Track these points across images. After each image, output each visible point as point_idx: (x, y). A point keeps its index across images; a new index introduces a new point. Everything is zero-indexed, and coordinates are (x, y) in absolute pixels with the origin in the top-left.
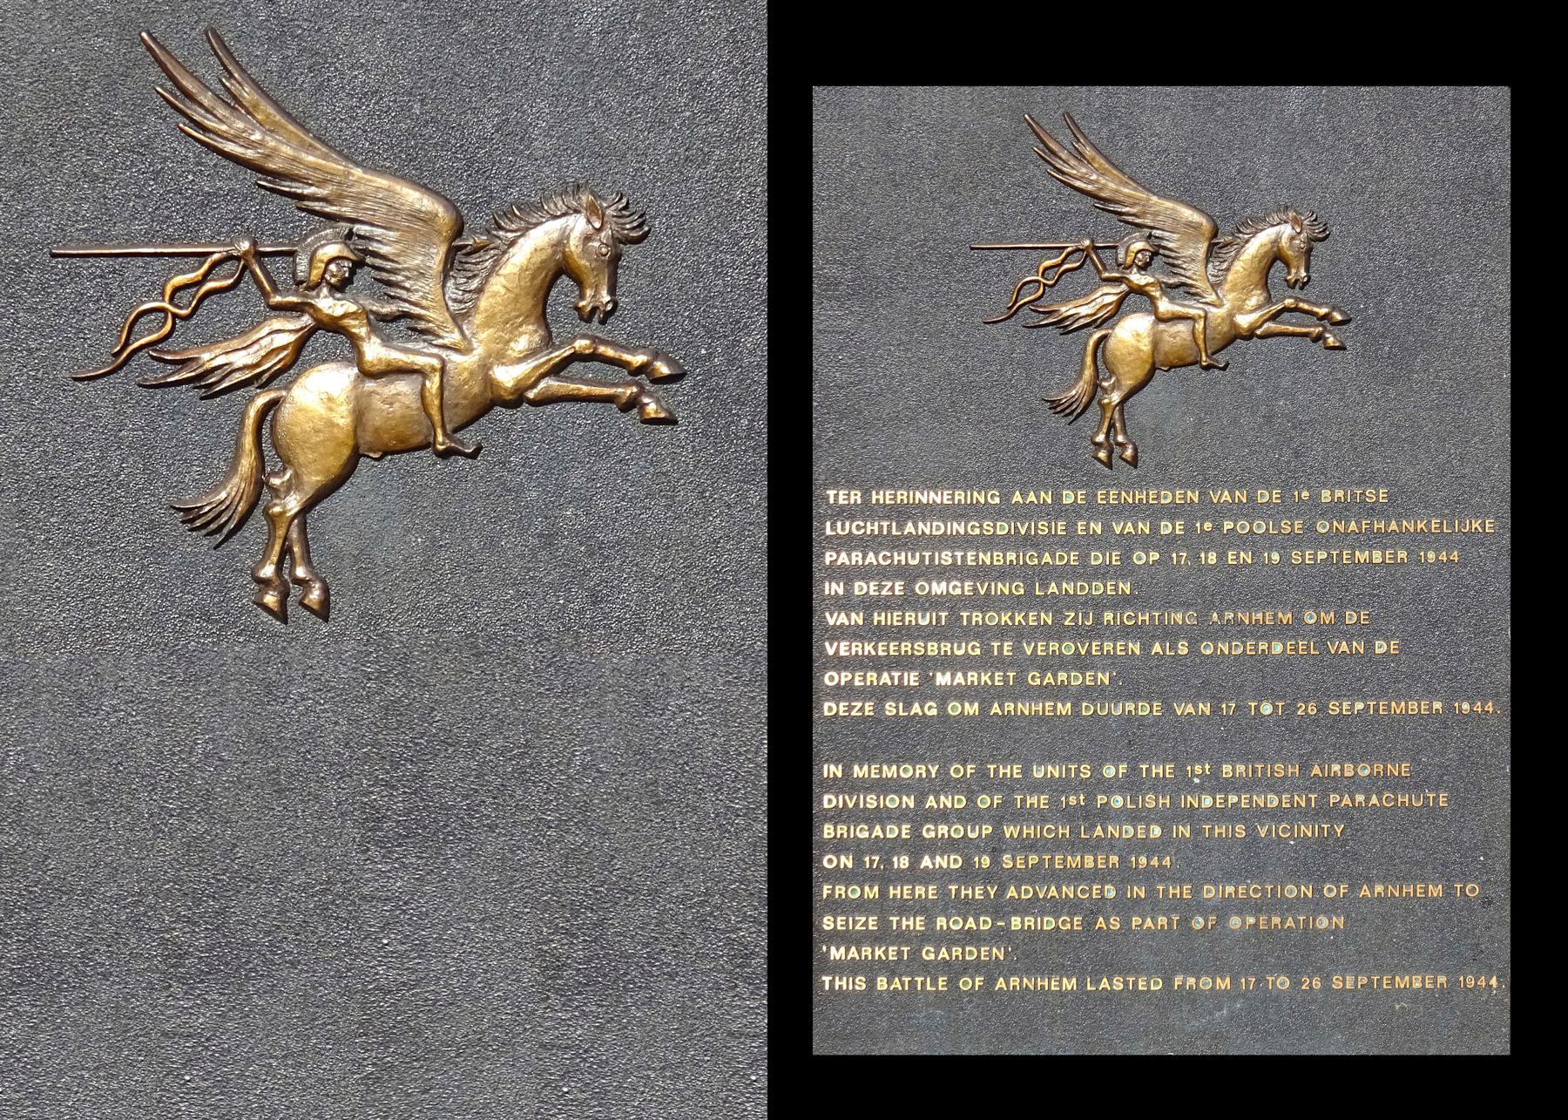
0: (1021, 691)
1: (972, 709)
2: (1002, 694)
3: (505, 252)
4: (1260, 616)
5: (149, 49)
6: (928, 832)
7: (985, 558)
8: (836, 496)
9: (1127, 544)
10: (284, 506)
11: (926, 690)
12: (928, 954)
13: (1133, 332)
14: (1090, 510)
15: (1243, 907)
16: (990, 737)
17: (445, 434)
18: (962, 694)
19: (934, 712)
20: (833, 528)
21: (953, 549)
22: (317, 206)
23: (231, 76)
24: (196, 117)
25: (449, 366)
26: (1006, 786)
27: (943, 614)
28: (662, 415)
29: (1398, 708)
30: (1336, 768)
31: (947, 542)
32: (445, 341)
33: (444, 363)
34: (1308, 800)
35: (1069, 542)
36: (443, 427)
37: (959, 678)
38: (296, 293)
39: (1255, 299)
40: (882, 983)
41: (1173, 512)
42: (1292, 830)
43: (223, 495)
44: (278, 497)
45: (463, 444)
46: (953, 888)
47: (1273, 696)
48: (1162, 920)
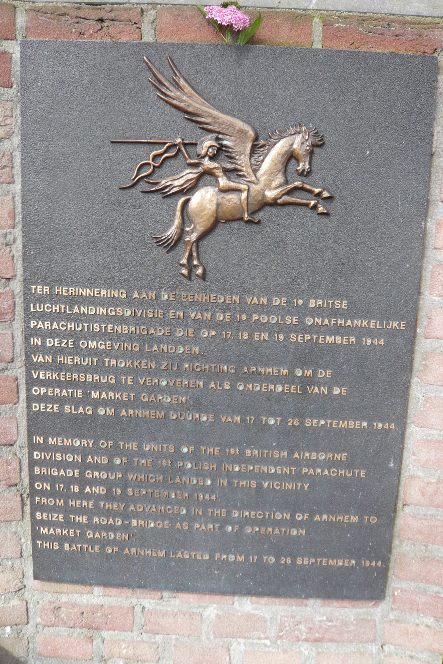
0: (136, 403)
1: (111, 412)
2: (126, 405)
3: (272, 147)
4: (270, 370)
5: (147, 64)
6: (89, 474)
7: (118, 328)
8: (36, 289)
9: (198, 325)
10: (190, 238)
11: (86, 400)
12: (89, 535)
13: (204, 199)
14: (175, 304)
15: (253, 522)
16: (117, 427)
17: (248, 215)
18: (105, 403)
19: (90, 412)
20: (34, 307)
21: (100, 323)
22: (206, 126)
23: (176, 75)
24: (163, 90)
25: (251, 189)
26: (129, 454)
27: (95, 359)
28: (325, 212)
29: (343, 424)
30: (307, 454)
31: (96, 318)
32: (249, 179)
33: (249, 187)
34: (291, 470)
35: (164, 321)
36: (248, 211)
37: (104, 395)
38: (197, 159)
39: (280, 179)
40: (67, 546)
41: (224, 307)
42: (281, 485)
43: (169, 233)
44: (188, 235)
45: (254, 219)
46: (102, 503)
47: (274, 415)
48: (211, 526)
